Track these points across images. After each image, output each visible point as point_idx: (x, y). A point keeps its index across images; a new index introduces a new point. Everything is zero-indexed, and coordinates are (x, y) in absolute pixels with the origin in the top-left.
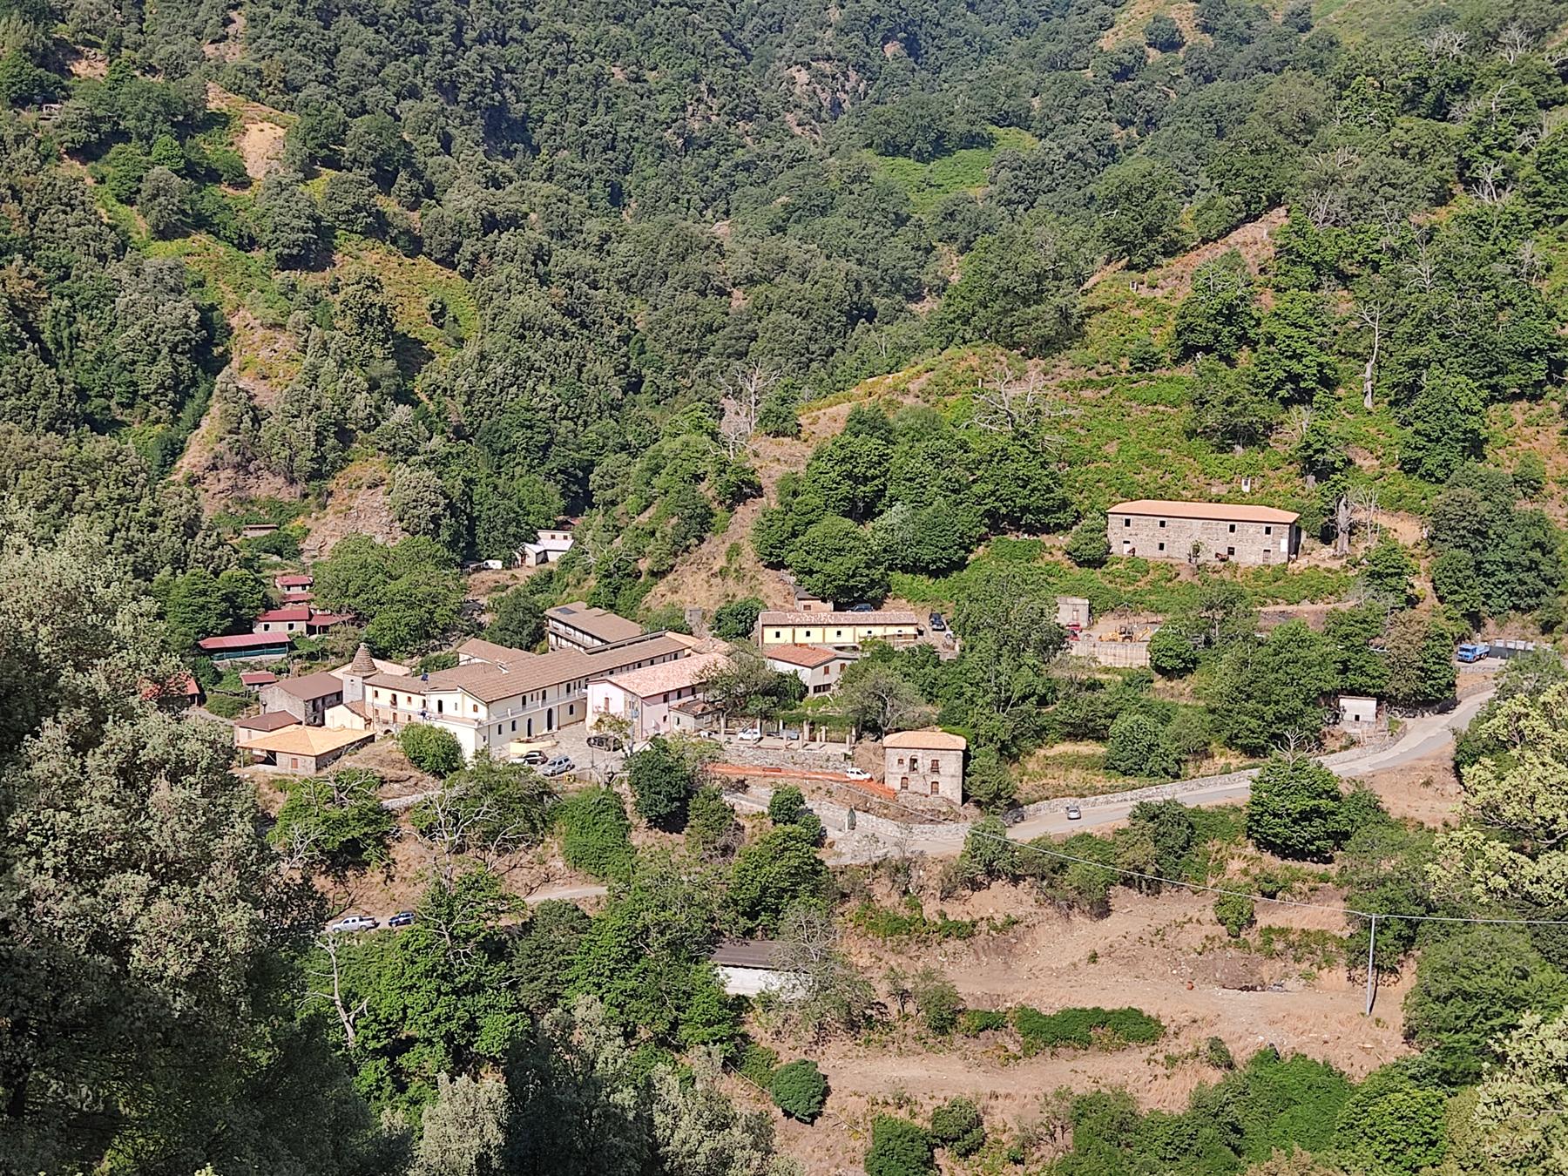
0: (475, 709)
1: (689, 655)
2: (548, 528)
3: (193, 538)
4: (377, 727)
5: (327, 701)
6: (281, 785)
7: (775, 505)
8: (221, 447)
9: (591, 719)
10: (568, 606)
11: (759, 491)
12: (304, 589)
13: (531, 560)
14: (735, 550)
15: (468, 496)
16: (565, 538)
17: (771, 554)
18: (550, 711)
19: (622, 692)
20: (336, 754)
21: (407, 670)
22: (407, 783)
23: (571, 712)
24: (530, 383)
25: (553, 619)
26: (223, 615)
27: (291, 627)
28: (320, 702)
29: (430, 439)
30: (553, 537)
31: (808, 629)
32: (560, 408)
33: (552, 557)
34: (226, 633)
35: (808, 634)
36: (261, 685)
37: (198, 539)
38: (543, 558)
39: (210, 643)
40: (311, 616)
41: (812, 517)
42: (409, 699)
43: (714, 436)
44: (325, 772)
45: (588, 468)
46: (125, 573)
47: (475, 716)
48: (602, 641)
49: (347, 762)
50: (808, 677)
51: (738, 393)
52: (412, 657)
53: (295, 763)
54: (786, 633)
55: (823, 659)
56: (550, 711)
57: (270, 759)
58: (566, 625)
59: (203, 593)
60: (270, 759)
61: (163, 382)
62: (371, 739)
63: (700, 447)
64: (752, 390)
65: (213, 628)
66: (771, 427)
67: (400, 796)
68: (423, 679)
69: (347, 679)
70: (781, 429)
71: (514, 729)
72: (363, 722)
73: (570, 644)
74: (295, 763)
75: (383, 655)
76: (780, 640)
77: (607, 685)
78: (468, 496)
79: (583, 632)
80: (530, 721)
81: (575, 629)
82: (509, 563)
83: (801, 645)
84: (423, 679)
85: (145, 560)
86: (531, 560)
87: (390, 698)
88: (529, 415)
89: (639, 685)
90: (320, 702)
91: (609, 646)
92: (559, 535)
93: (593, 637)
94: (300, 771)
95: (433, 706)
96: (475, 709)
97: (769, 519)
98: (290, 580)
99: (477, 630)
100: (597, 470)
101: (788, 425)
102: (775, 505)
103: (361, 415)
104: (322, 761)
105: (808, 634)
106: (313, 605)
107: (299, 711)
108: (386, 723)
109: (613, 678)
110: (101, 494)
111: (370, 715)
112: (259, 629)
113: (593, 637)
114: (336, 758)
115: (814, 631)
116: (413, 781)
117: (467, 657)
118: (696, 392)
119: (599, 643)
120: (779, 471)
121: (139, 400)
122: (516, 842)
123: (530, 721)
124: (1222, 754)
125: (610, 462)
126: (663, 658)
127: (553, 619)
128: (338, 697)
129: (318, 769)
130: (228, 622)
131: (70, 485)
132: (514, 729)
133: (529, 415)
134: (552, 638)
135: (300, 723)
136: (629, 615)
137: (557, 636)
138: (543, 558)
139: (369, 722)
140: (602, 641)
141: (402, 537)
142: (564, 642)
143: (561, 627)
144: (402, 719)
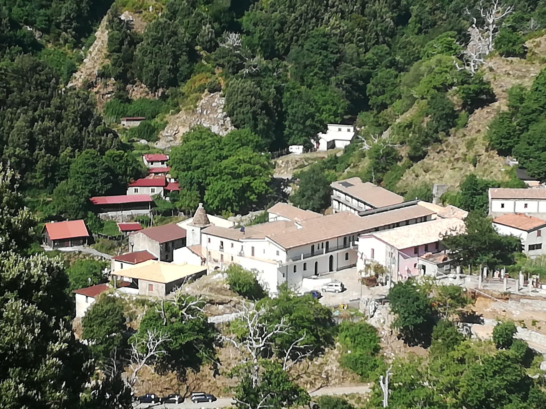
0: (278, 253)
1: (435, 219)
2: (336, 123)
3: (87, 126)
4: (209, 264)
5: (175, 244)
6: (143, 302)
7: (505, 109)
8: (108, 62)
9: (360, 265)
10: (348, 181)
11: (492, 98)
12: (163, 163)
13: (323, 146)
14: (470, 145)
15: (278, 102)
16: (349, 130)
17: (501, 143)
18: (331, 257)
19: (385, 245)
20: (179, 283)
21: (232, 225)
22: (229, 305)
23: (347, 259)
24: (326, 17)
25: (336, 190)
26: (106, 181)
27: (153, 191)
28: (170, 245)
29: (254, 57)
30: (340, 130)
31: (526, 202)
32: (346, 34)
33: (340, 145)
34: (109, 193)
35: (526, 205)
36: (131, 231)
37: (90, 128)
38: (331, 145)
39: (100, 200)
40: (167, 183)
41: (533, 116)
42: (232, 244)
43: (461, 57)
44: (172, 294)
45: (367, 78)
46: (41, 150)
47: (278, 258)
48: (371, 207)
49: (187, 289)
50: (527, 239)
51: (481, 23)
52: (236, 215)
53: (151, 287)
54: (509, 204)
55: (536, 225)
56: (331, 257)
57: (134, 284)
58: (346, 194)
59: (94, 166)
60: (134, 284)
61: (69, 15)
62: (205, 272)
63: (449, 64)
64: (491, 21)
65: (99, 189)
66: (504, 49)
67: (223, 313)
68: (241, 231)
69: (189, 229)
70: (511, 50)
71: (305, 269)
72: (201, 261)
73: (348, 209)
74: (151, 287)
75: (217, 212)
76: (503, 210)
77: (373, 239)
78: (278, 102)
79: (358, 200)
80: (316, 263)
81: (352, 197)
82: (308, 148)
83: (520, 214)
84: (241, 231)
85: (53, 140)
86: (323, 146)
87: (220, 244)
88: (325, 39)
89: (396, 240)
90: (170, 245)
91: (375, 211)
92: (344, 128)
93: (365, 204)
94: (155, 293)
95: (248, 252)
96: (278, 253)
97: (503, 118)
98: (152, 157)
99: (285, 198)
100: (372, 81)
101: (517, 48)
102: (505, 109)
103: (206, 38)
104: (170, 287)
105: (526, 205)
106: (168, 176)
107: (155, 250)
108: (216, 261)
109: (376, 234)
110: (27, 93)
111: (205, 256)
112: (131, 191)
113: (365, 204)
114: (180, 286)
115: (530, 203)
116: (232, 304)
117: (275, 216)
118: (450, 23)
119: (370, 208)
120: (510, 83)
121: (53, 27)
122: (304, 351)
123: (316, 263)
124: (85, 78)
125: (382, 73)
126: (416, 221)
127: (336, 190)
128: (182, 242)
129: (167, 293)
130: (109, 186)
131: (4, 87)
132: (305, 269)
133: (325, 39)
134: (335, 203)
135: (157, 259)
136: (390, 188)
137: (339, 202)
138: (331, 145)
139: (204, 261)
140: (371, 207)
141: (231, 128)
142: (344, 208)
143: (343, 196)
144: (227, 258)
